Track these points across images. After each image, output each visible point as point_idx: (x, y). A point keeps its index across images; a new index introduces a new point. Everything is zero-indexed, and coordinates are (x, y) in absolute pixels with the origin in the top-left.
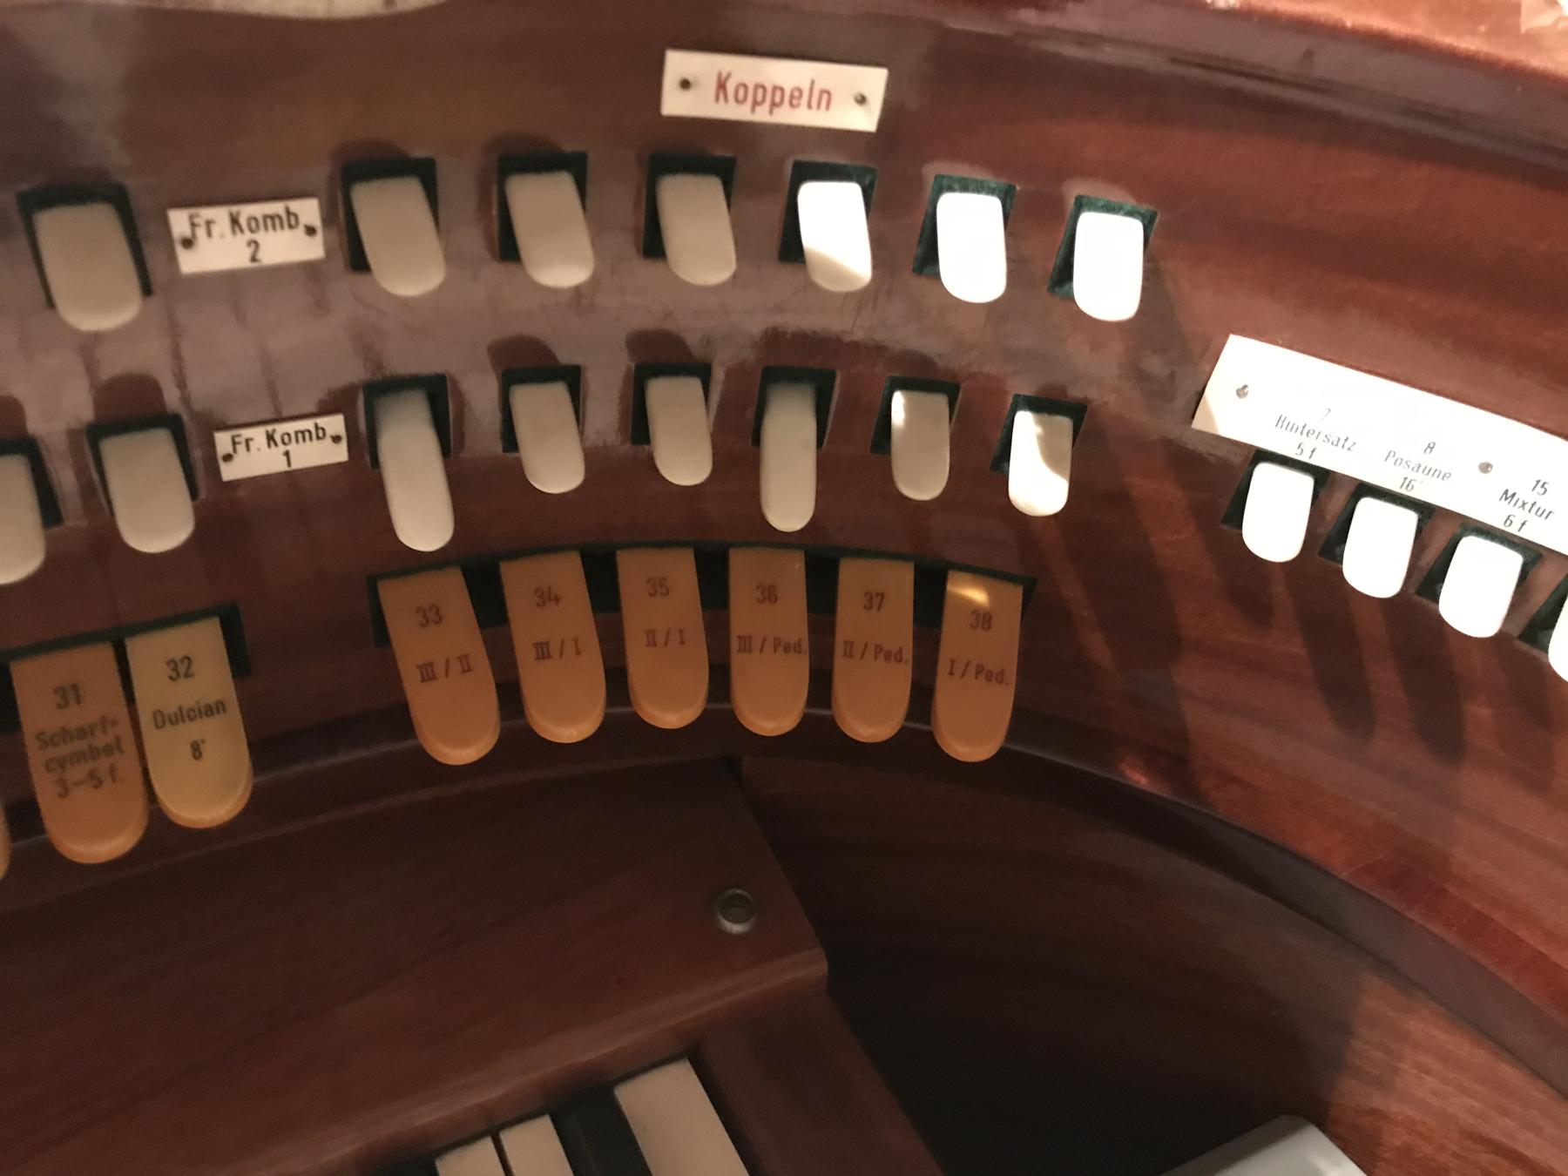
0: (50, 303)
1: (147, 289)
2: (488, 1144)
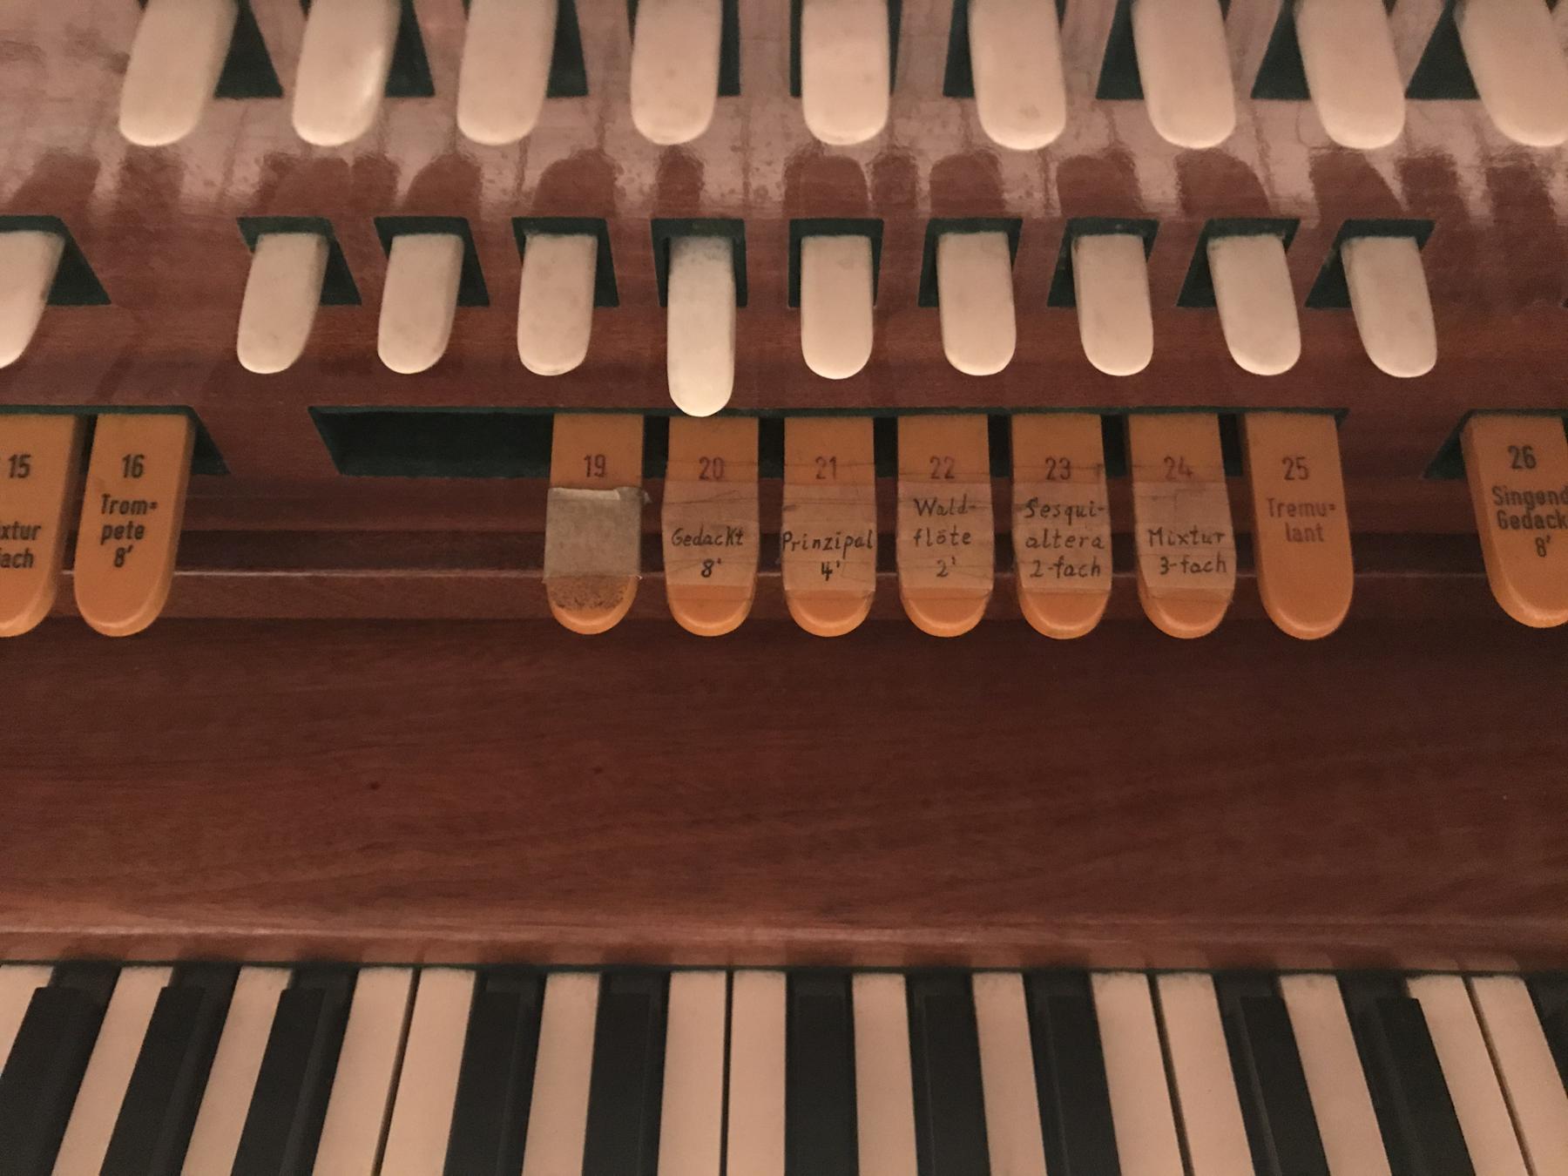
0: (796, 90)
1: (729, 83)
2: (721, 978)
